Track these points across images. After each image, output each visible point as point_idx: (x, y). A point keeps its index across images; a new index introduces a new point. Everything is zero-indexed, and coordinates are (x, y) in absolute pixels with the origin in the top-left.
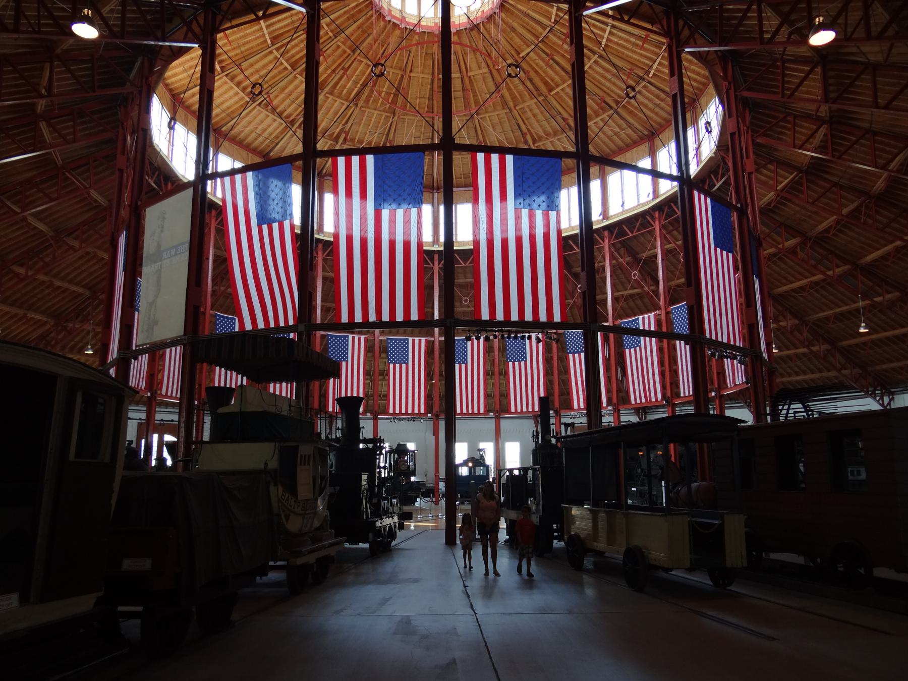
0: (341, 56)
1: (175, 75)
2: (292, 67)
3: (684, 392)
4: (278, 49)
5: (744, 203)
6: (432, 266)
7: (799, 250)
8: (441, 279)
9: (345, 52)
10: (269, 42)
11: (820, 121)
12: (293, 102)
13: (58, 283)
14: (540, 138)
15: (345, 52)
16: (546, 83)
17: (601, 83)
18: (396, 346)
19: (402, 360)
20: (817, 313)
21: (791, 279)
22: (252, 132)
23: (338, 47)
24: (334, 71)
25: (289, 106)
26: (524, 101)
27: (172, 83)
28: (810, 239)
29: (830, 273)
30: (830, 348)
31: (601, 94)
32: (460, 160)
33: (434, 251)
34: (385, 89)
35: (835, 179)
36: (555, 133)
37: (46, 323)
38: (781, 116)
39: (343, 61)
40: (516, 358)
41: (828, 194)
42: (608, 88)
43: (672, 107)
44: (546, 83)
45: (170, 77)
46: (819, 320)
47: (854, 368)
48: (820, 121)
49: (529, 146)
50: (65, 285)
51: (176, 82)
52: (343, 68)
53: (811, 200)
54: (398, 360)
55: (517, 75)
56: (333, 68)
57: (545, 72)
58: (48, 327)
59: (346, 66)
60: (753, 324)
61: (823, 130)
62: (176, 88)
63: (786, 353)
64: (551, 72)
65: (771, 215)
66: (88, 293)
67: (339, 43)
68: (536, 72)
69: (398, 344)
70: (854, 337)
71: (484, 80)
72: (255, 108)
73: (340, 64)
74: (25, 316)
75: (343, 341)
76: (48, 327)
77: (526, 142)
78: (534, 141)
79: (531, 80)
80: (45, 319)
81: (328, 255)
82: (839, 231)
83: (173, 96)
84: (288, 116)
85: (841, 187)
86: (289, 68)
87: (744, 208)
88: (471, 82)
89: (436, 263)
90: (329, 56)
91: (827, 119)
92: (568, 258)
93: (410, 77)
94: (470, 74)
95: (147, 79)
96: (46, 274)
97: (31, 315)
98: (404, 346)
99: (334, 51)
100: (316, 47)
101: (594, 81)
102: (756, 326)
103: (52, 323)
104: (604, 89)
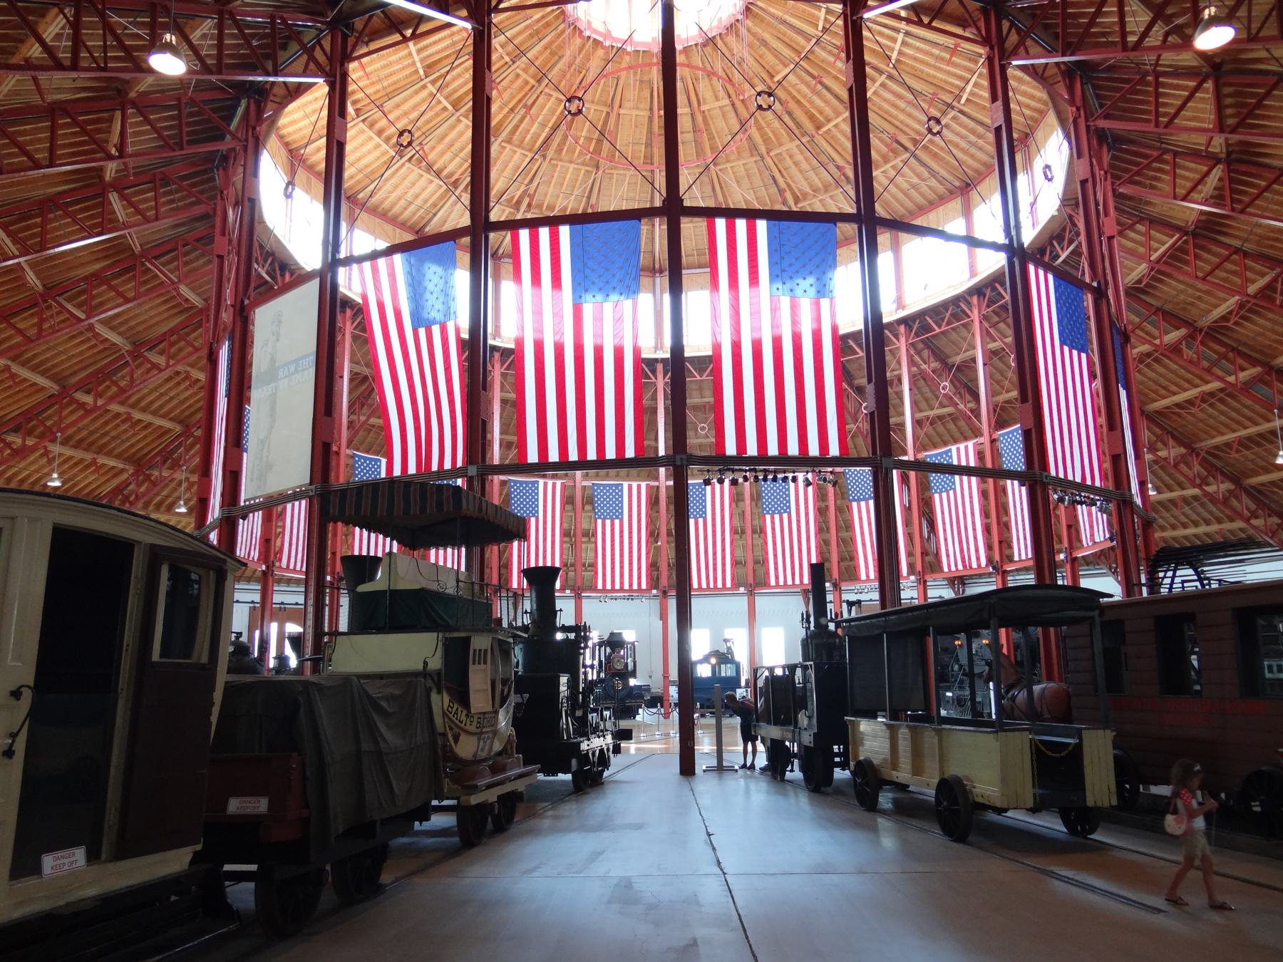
0: (521, 89)
3: (1020, 555)
4: (433, 82)
7: (1184, 346)
9: (527, 83)
10: (421, 72)
13: (137, 415)
14: (805, 196)
15: (527, 83)
16: (812, 118)
17: (891, 116)
18: (605, 494)
19: (614, 514)
21: (1174, 388)
23: (518, 76)
24: (512, 110)
26: (781, 145)
27: (289, 134)
28: (1201, 330)
31: (891, 130)
32: (691, 229)
33: (656, 360)
37: (122, 471)
38: (1155, 154)
39: (524, 96)
40: (776, 509)
42: (902, 122)
44: (812, 118)
45: (285, 126)
46: (1217, 447)
47: (1270, 516)
48: (1214, 160)
50: (147, 418)
51: (295, 132)
53: (1200, 274)
54: (608, 514)
55: (770, 107)
56: (511, 105)
57: (811, 102)
58: (124, 476)
61: (1217, 172)
62: (295, 142)
65: (1143, 297)
66: (178, 429)
67: (519, 71)
68: (798, 102)
69: (608, 491)
70: (1267, 471)
72: (403, 165)
73: (520, 101)
74: (94, 462)
75: (614, 491)
76: (124, 476)
77: (784, 202)
78: (797, 200)
79: (790, 114)
80: (121, 466)
81: (508, 368)
83: (290, 151)
85: (1246, 255)
86: (450, 108)
87: (1103, 287)
88: (705, 119)
89: (660, 376)
91: (1223, 156)
94: (703, 108)
96: (122, 403)
97: (102, 460)
98: (617, 494)
99: (512, 82)
102: (1123, 456)
103: (131, 472)
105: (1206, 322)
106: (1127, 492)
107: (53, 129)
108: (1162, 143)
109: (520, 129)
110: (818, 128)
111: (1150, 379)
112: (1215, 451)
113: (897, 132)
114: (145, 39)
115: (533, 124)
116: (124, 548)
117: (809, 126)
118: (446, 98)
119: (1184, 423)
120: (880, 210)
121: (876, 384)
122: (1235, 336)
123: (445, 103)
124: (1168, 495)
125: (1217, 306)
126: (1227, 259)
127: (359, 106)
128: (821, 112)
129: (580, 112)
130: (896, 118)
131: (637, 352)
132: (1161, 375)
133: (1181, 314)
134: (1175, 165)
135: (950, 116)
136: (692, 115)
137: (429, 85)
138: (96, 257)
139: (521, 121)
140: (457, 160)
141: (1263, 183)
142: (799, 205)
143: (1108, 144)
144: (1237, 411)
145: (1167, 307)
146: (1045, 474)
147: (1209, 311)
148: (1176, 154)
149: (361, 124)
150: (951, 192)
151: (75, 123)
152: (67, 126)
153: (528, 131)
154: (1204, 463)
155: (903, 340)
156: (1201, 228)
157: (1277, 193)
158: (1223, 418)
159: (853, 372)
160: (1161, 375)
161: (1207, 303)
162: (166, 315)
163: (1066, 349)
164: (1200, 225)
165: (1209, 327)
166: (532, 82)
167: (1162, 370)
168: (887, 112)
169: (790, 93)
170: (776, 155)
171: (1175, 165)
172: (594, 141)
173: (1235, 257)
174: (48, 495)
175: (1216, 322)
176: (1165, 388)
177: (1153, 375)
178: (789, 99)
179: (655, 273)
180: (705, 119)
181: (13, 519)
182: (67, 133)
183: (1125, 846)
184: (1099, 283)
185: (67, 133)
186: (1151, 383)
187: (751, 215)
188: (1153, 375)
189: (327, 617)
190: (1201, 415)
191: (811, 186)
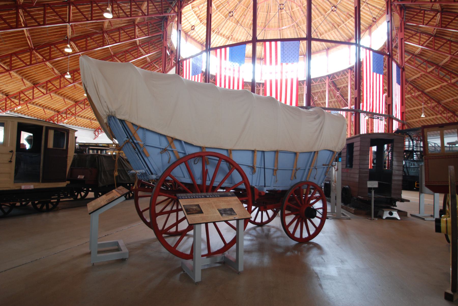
0: (243, 11)
1: (185, 26)
2: (225, 17)
4: (219, 11)
5: (391, 53)
6: (259, 88)
8: (362, 96)
9: (244, 8)
10: (215, 9)
11: (437, 11)
12: (227, 31)
14: (323, 34)
15: (244, 8)
16: (324, 10)
17: (347, 7)
20: (446, 99)
21: (433, 85)
22: (214, 44)
23: (241, 7)
24: (241, 16)
25: (227, 32)
26: (315, 19)
27: (185, 29)
28: (440, 66)
29: (413, 94)
30: (452, 114)
31: (347, 11)
32: (259, 47)
33: (261, 83)
34: (261, 21)
35: (449, 38)
36: (329, 31)
38: (418, 11)
39: (244, 12)
41: (445, 45)
42: (350, 8)
43: (355, 14)
44: (324, 10)
45: (183, 27)
46: (447, 102)
48: (437, 11)
49: (319, 37)
51: (186, 28)
52: (244, 15)
53: (436, 48)
55: (283, 8)
56: (240, 15)
57: (323, 5)
59: (245, 14)
60: (390, 104)
61: (439, 15)
62: (187, 31)
63: (428, 118)
64: (325, 4)
65: (422, 57)
67: (241, 5)
68: (320, 5)
71: (299, 11)
72: (214, 34)
73: (243, 14)
77: (317, 36)
78: (321, 35)
79: (318, 9)
82: (452, 61)
83: (186, 34)
84: (227, 36)
85: (452, 41)
86: (224, 18)
87: (391, 54)
88: (294, 13)
89: (261, 87)
90: (238, 11)
91: (440, 10)
92: (335, 82)
93: (270, 15)
94: (293, 10)
95: (165, 29)
99: (240, 9)
100: (210, 8)
101: (344, 6)
102: (391, 105)
104: (349, 9)
105: (441, 64)
106: (391, 115)
107: (119, 34)
108: (421, 7)
109: (243, 22)
110: (326, 12)
111: (425, 82)
112: (447, 104)
113: (349, 11)
114: (133, 8)
115: (247, 20)
116: (42, 127)
117: (323, 12)
118: (223, 15)
119: (436, 95)
120: (313, 36)
121: (307, 86)
122: (452, 68)
123: (223, 17)
124: (428, 118)
125: (445, 59)
126: (446, 43)
127: (201, 20)
128: (326, 8)
129: (232, 15)
130: (348, 7)
131: (243, 80)
132: (429, 81)
133: (434, 62)
134: (424, 14)
135: (364, 5)
136: (267, 15)
137: (218, 12)
138: (141, 63)
139: (244, 19)
140: (228, 32)
141: (453, 18)
142: (322, 36)
143: (404, 9)
144: (453, 91)
145: (429, 60)
146: (359, 110)
147: (442, 61)
148: (425, 10)
149: (202, 25)
150: (366, 28)
151: (125, 32)
152: (123, 33)
153: (246, 22)
154: (443, 107)
155: (349, 74)
156: (438, 34)
157: (457, 20)
158: (449, 93)
159: (336, 84)
160: (429, 81)
161: (442, 58)
162: (45, 76)
163: (375, 74)
164: (438, 33)
165: (442, 65)
166: (246, 8)
167: (429, 79)
168: (346, 6)
169: (317, 3)
170: (314, 22)
171: (424, 14)
172: (264, 23)
173: (448, 42)
174: (388, 124)
175: (445, 63)
176: (430, 85)
177: (426, 81)
178: (317, 5)
179: (179, 62)
180: (294, 13)
181: (7, 121)
182: (123, 34)
183: (149, 195)
184: (390, 53)
185: (123, 34)
186: (426, 83)
187: (276, 40)
188: (426, 81)
189: (65, 142)
190: (442, 93)
191: (325, 30)
